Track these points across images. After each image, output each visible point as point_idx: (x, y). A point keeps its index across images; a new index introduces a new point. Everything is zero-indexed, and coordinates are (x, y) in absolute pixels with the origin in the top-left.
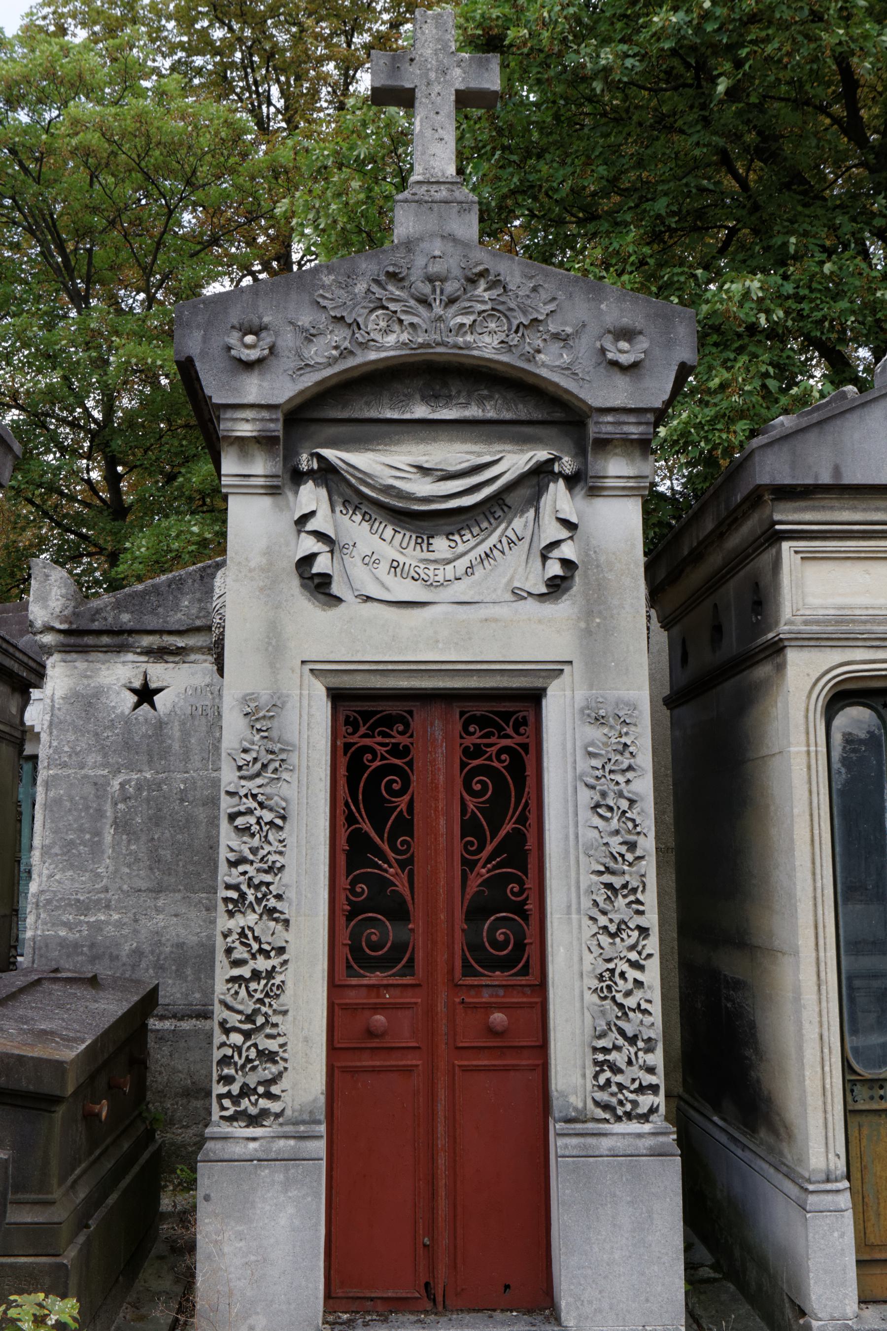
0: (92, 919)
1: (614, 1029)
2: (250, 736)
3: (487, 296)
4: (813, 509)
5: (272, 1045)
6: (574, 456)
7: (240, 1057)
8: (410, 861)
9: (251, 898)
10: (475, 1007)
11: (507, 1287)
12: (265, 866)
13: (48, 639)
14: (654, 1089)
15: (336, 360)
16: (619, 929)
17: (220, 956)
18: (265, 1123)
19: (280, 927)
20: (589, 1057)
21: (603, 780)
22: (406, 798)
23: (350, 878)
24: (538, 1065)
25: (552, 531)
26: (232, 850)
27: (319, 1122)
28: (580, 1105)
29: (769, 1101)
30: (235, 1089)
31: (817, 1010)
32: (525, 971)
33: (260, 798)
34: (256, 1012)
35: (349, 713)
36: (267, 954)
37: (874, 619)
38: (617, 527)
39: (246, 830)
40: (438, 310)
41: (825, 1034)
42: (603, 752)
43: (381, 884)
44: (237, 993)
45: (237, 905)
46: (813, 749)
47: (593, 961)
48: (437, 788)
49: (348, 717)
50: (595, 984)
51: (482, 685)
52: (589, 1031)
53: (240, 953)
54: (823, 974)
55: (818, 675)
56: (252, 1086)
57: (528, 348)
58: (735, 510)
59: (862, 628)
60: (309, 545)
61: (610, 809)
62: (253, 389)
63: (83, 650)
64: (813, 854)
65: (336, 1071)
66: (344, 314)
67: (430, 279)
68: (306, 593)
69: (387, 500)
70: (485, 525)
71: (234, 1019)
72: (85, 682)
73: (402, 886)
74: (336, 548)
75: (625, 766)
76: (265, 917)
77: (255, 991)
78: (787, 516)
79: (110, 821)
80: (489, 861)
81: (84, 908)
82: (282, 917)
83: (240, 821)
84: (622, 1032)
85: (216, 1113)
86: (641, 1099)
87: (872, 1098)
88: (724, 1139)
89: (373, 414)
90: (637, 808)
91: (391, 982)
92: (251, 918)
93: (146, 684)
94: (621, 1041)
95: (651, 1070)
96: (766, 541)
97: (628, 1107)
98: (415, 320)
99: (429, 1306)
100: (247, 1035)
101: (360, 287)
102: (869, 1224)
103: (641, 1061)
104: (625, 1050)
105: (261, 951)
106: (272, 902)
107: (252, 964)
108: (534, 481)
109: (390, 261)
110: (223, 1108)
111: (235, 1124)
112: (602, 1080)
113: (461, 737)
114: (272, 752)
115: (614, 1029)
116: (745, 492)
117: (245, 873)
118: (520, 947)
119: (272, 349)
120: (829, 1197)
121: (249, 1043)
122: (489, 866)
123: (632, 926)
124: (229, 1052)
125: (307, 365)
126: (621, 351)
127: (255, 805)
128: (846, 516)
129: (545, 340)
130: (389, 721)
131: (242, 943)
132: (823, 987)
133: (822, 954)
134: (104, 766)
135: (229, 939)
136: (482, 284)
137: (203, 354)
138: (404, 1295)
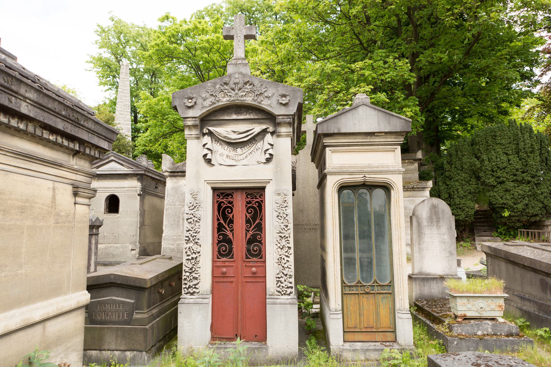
3: (249, 87)
4: (334, 139)
5: (197, 276)
8: (233, 230)
9: (191, 239)
10: (249, 266)
14: (292, 287)
19: (199, 247)
20: (275, 279)
22: (232, 214)
25: (268, 147)
30: (187, 286)
32: (261, 258)
34: (192, 267)
36: (195, 253)
40: (237, 91)
43: (225, 236)
45: (188, 241)
50: (277, 261)
53: (189, 253)
60: (206, 151)
62: (191, 113)
67: (235, 84)
71: (187, 269)
73: (231, 237)
78: (327, 141)
80: (252, 230)
83: (189, 221)
84: (283, 273)
89: (223, 118)
90: (288, 217)
92: (190, 245)
94: (283, 276)
95: (291, 283)
97: (285, 292)
98: (231, 94)
100: (190, 273)
101: (218, 86)
106: (197, 241)
107: (192, 256)
108: (263, 133)
109: (226, 79)
112: (278, 285)
118: (260, 251)
119: (195, 103)
120: (335, 315)
124: (186, 277)
130: (228, 195)
136: (248, 84)
137: (179, 105)
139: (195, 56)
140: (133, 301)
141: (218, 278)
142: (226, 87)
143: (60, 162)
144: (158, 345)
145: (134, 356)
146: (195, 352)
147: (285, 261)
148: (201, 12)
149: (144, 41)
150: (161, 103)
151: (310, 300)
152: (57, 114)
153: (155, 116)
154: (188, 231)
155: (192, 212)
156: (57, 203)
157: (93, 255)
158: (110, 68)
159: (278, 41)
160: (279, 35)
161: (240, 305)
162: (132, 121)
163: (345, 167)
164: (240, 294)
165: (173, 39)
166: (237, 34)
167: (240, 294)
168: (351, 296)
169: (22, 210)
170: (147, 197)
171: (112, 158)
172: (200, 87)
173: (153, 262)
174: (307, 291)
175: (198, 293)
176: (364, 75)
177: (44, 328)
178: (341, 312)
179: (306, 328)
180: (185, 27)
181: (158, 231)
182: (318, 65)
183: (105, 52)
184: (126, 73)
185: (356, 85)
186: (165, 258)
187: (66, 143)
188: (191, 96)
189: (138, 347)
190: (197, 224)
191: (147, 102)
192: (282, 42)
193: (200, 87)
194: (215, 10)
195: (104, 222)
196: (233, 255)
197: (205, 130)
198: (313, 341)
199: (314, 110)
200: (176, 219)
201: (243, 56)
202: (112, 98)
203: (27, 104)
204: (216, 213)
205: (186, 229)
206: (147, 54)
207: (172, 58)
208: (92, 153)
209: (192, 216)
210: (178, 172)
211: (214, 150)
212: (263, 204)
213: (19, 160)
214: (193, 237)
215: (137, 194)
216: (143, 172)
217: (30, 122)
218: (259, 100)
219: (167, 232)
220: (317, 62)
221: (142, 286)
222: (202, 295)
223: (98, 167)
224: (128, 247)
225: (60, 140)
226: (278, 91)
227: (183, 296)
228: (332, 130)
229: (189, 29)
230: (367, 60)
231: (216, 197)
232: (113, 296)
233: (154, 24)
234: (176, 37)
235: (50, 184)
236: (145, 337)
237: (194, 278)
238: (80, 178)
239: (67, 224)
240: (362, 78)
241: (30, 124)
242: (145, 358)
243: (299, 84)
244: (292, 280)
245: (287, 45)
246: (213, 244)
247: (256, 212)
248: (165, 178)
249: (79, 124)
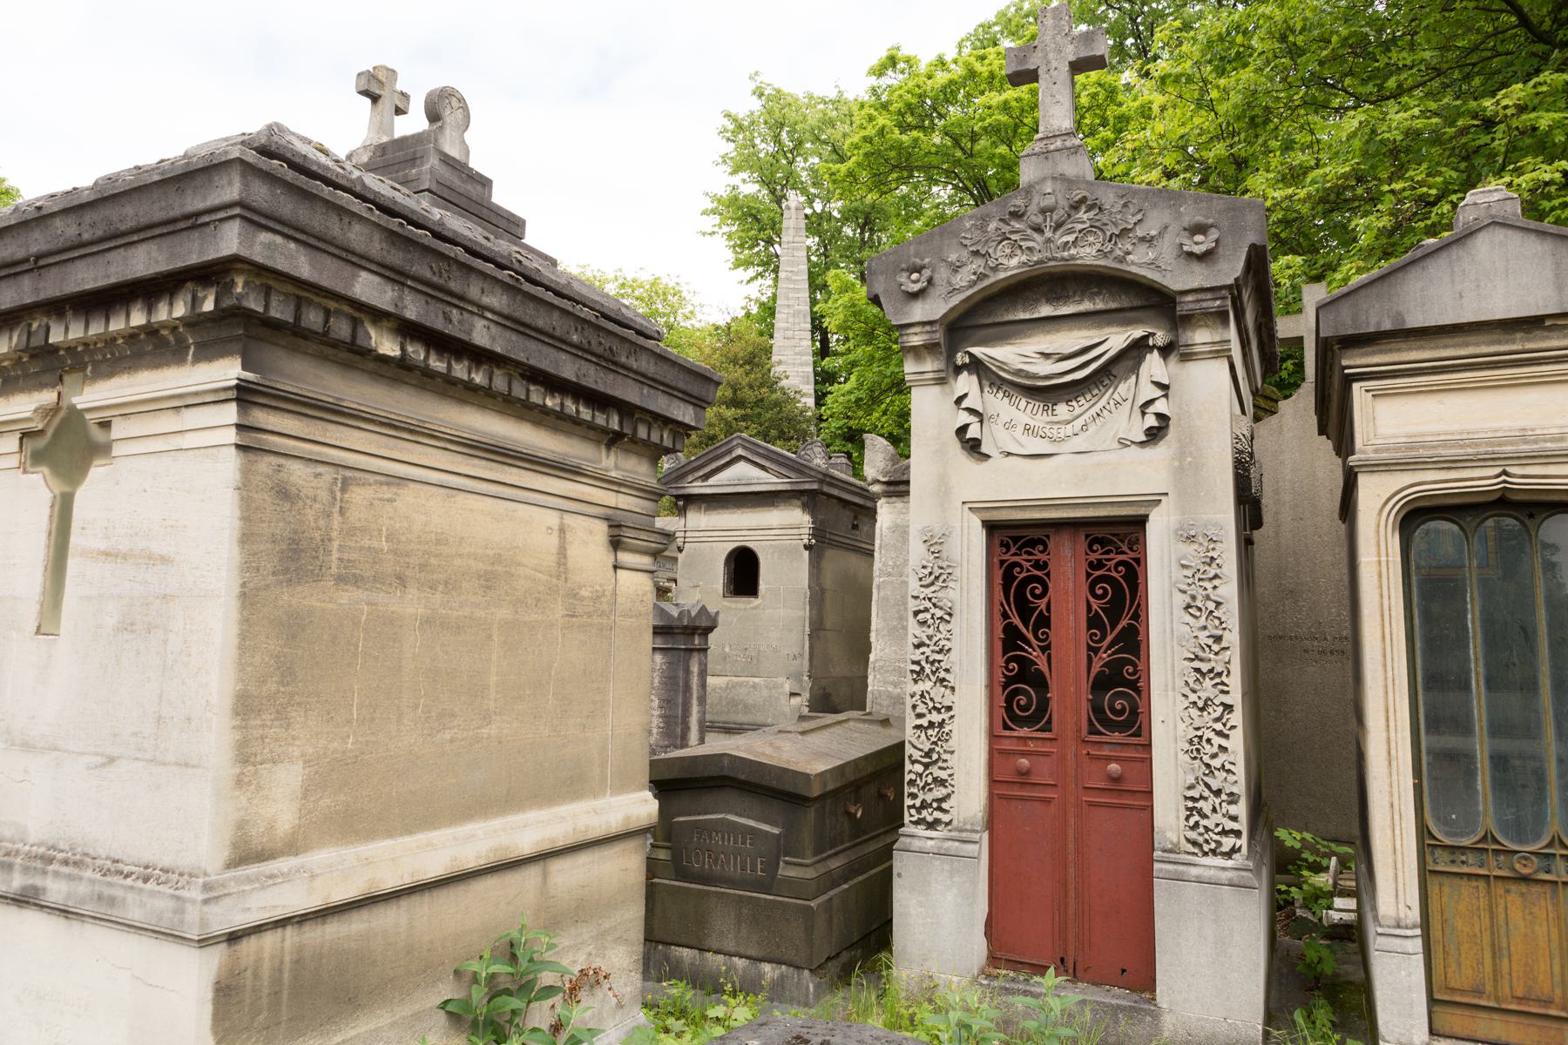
3: (1085, 217)
4: (1381, 352)
5: (943, 775)
8: (1048, 647)
9: (928, 671)
10: (1098, 758)
14: (1238, 834)
15: (975, 283)
16: (1205, 704)
17: (909, 709)
19: (948, 692)
22: (1045, 600)
25: (1150, 392)
28: (1175, 840)
30: (918, 803)
32: (1137, 734)
34: (931, 750)
36: (939, 711)
37: (1445, 443)
39: (923, 623)
41: (1396, 803)
43: (1025, 663)
45: (919, 675)
46: (1383, 559)
53: (921, 709)
54: (1393, 752)
59: (1430, 453)
61: (1200, 609)
62: (919, 312)
67: (1043, 211)
70: (1096, 391)
71: (917, 755)
73: (1042, 665)
78: (1353, 361)
80: (1109, 648)
83: (921, 616)
84: (1207, 786)
85: (907, 819)
86: (1224, 840)
87: (1453, 862)
89: (1011, 317)
90: (1223, 608)
92: (927, 685)
94: (1207, 793)
95: (1234, 819)
97: (1213, 845)
98: (1031, 244)
100: (926, 766)
101: (992, 226)
102: (1450, 971)
106: (942, 674)
107: (929, 717)
108: (1135, 353)
109: (1018, 202)
112: (1192, 822)
118: (1134, 712)
119: (930, 281)
120: (1398, 941)
128: (1555, 343)
130: (1033, 543)
132: (1394, 764)
133: (1392, 735)
136: (1083, 209)
137: (886, 291)
139: (971, 155)
140: (776, 831)
141: (1005, 785)
142: (1017, 225)
143: (575, 462)
144: (845, 956)
145: (782, 977)
146: (940, 992)
147: (1215, 749)
148: (986, 27)
149: (838, 136)
151: (1323, 880)
152: (558, 342)
153: (869, 336)
154: (917, 646)
155: (928, 591)
156: (569, 565)
157: (695, 702)
158: (758, 220)
159: (1216, 69)
160: (1219, 48)
161: (1071, 871)
164: (1071, 836)
165: (909, 119)
166: (1049, 62)
167: (1071, 836)
168: (1457, 881)
169: (488, 581)
170: (830, 553)
171: (740, 451)
172: (941, 234)
173: (837, 730)
174: (1316, 852)
176: (1534, 129)
177: (545, 876)
178: (1418, 932)
179: (1300, 968)
180: (941, 78)
181: (860, 648)
182: (1352, 121)
183: (744, 181)
184: (797, 229)
185: (1503, 168)
187: (586, 414)
191: (846, 298)
192: (1228, 67)
193: (941, 234)
194: (1027, 16)
195: (721, 619)
196: (1049, 722)
198: (1323, 1015)
199: (1344, 269)
201: (1067, 124)
202: (764, 299)
203: (486, 323)
204: (999, 594)
205: (912, 640)
206: (842, 168)
207: (910, 169)
208: (655, 438)
209: (928, 605)
211: (990, 411)
213: (477, 461)
216: (815, 486)
217: (498, 367)
218: (1118, 252)
219: (880, 649)
220: (1352, 113)
222: (961, 831)
223: (706, 477)
225: (571, 407)
227: (909, 829)
229: (952, 82)
230: (1546, 76)
231: (998, 550)
232: (730, 812)
233: (858, 87)
234: (919, 111)
235: (552, 518)
238: (626, 501)
239: (596, 620)
240: (1528, 141)
241: (497, 372)
243: (1290, 191)
244: (1241, 809)
245: (1246, 75)
246: (990, 686)
248: (874, 498)
249: (615, 363)
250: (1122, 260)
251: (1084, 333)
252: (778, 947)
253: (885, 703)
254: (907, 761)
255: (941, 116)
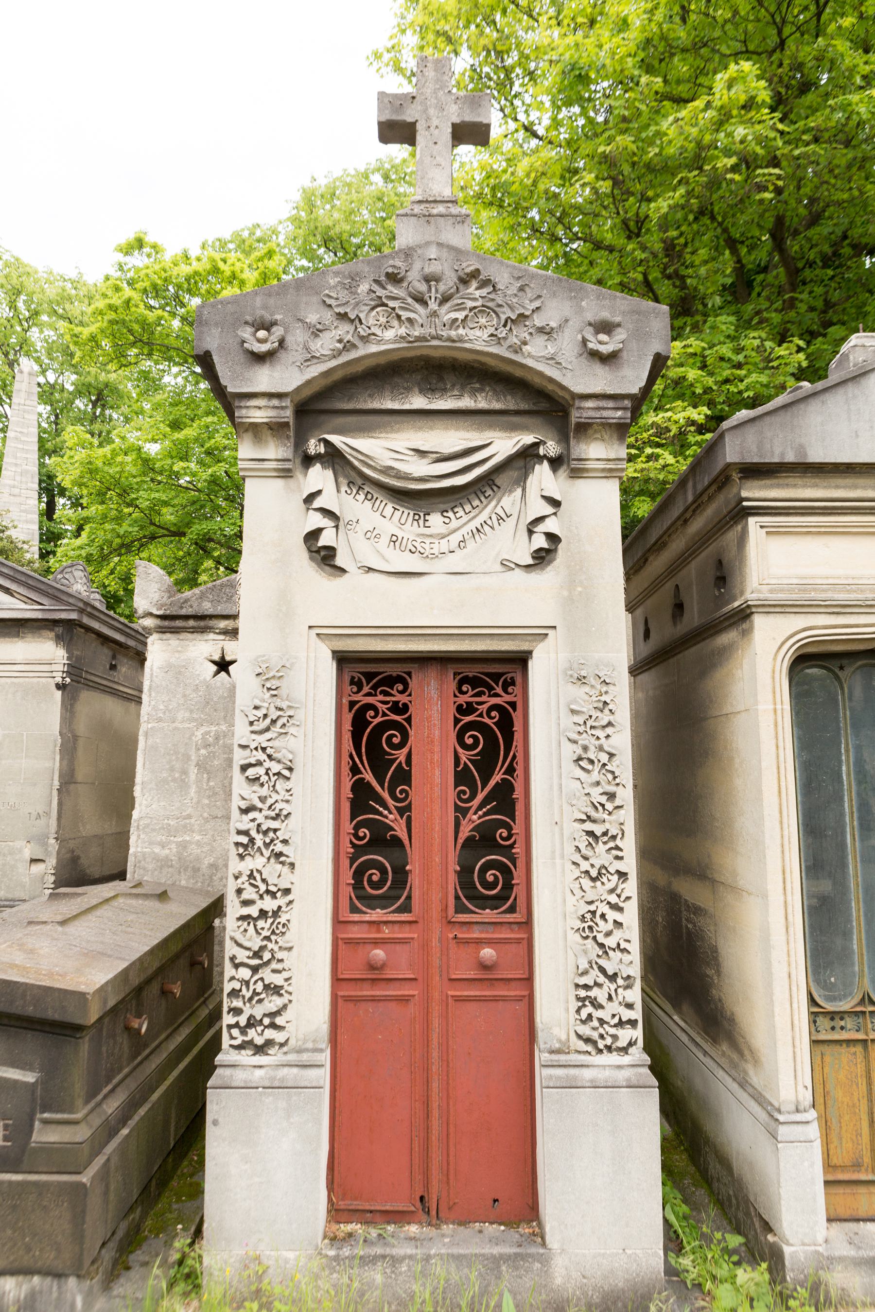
0: (180, 839)
1: (595, 966)
2: (261, 694)
3: (478, 293)
4: (778, 486)
5: (278, 979)
6: (558, 442)
7: (248, 990)
8: (409, 808)
9: (259, 843)
10: (467, 942)
11: (495, 1201)
12: (273, 814)
13: (149, 622)
14: (633, 1023)
16: (599, 873)
18: (270, 1052)
19: (286, 869)
20: (572, 992)
21: (585, 735)
22: (405, 751)
23: (354, 822)
24: (524, 996)
26: (243, 799)
27: (321, 1051)
28: (564, 1037)
29: (732, 1020)
30: (243, 1020)
31: (785, 950)
32: (512, 910)
33: (269, 751)
34: (263, 948)
35: (355, 674)
36: (273, 895)
38: (593, 510)
42: (584, 710)
44: (246, 930)
45: (246, 848)
47: (576, 903)
48: (432, 742)
49: (353, 678)
50: (579, 924)
51: (473, 648)
52: (572, 969)
53: (249, 894)
55: (783, 639)
56: (258, 1018)
57: (515, 340)
58: (701, 494)
59: (823, 596)
60: (316, 520)
61: (591, 762)
62: (264, 379)
63: (175, 631)
64: (780, 805)
65: (340, 1000)
66: (348, 310)
67: (427, 279)
68: (313, 564)
69: (387, 480)
70: (476, 503)
71: (242, 956)
72: (177, 655)
73: (401, 831)
74: (341, 524)
75: (604, 723)
76: (272, 860)
77: (263, 929)
78: (754, 492)
79: (194, 763)
80: (480, 808)
81: (171, 832)
82: (288, 860)
83: (251, 772)
84: (602, 970)
85: (226, 1041)
86: (620, 1032)
88: (684, 1038)
89: (376, 405)
90: (616, 761)
91: (390, 919)
92: (256, 862)
93: (223, 657)
94: (601, 979)
95: (630, 1006)
96: (731, 519)
97: (609, 1041)
98: (412, 315)
99: (424, 1217)
100: (255, 969)
101: (364, 288)
102: (831, 1146)
103: (621, 998)
104: (605, 987)
105: (268, 892)
106: (279, 847)
107: (260, 905)
108: (520, 463)
110: (232, 1038)
111: (243, 1052)
112: (584, 1014)
113: (455, 696)
114: (280, 709)
115: (595, 966)
116: (715, 473)
117: (253, 820)
118: (508, 886)
119: (282, 342)
120: (799, 1128)
121: (256, 977)
122: (480, 813)
123: (612, 871)
124: (237, 986)
125: (313, 357)
126: (600, 343)
127: (265, 757)
129: (531, 334)
130: (390, 681)
131: (251, 884)
134: (192, 720)
135: (240, 881)
136: (474, 284)
137: (221, 348)
138: (401, 1209)
140: (30, 1077)
141: (354, 983)
144: (123, 1226)
147: (610, 926)
150: (119, 459)
153: (101, 496)
154: (245, 811)
155: (262, 739)
161: (435, 1085)
162: (41, 515)
163: (815, 587)
166: (428, 119)
168: (837, 1048)
173: (105, 912)
175: (282, 1045)
180: (185, 270)
181: (119, 800)
184: (29, 393)
186: (146, 896)
188: (268, 317)
189: (49, 1258)
190: (281, 785)
196: (409, 897)
197: (312, 442)
200: (178, 765)
205: (236, 803)
209: (262, 756)
210: (187, 617)
211: (346, 516)
212: (517, 717)
214: (265, 833)
215: (52, 683)
216: (74, 616)
221: (69, 1019)
222: (299, 1051)
224: (20, 851)
226: (580, 310)
228: (777, 451)
229: (196, 273)
231: (348, 688)
236: (78, 1217)
237: (267, 987)
242: (73, 1305)
247: (493, 744)
250: (517, 350)
251: (463, 434)
252: (28, 1249)
253: (150, 867)
254: (227, 964)
255: (183, 305)
